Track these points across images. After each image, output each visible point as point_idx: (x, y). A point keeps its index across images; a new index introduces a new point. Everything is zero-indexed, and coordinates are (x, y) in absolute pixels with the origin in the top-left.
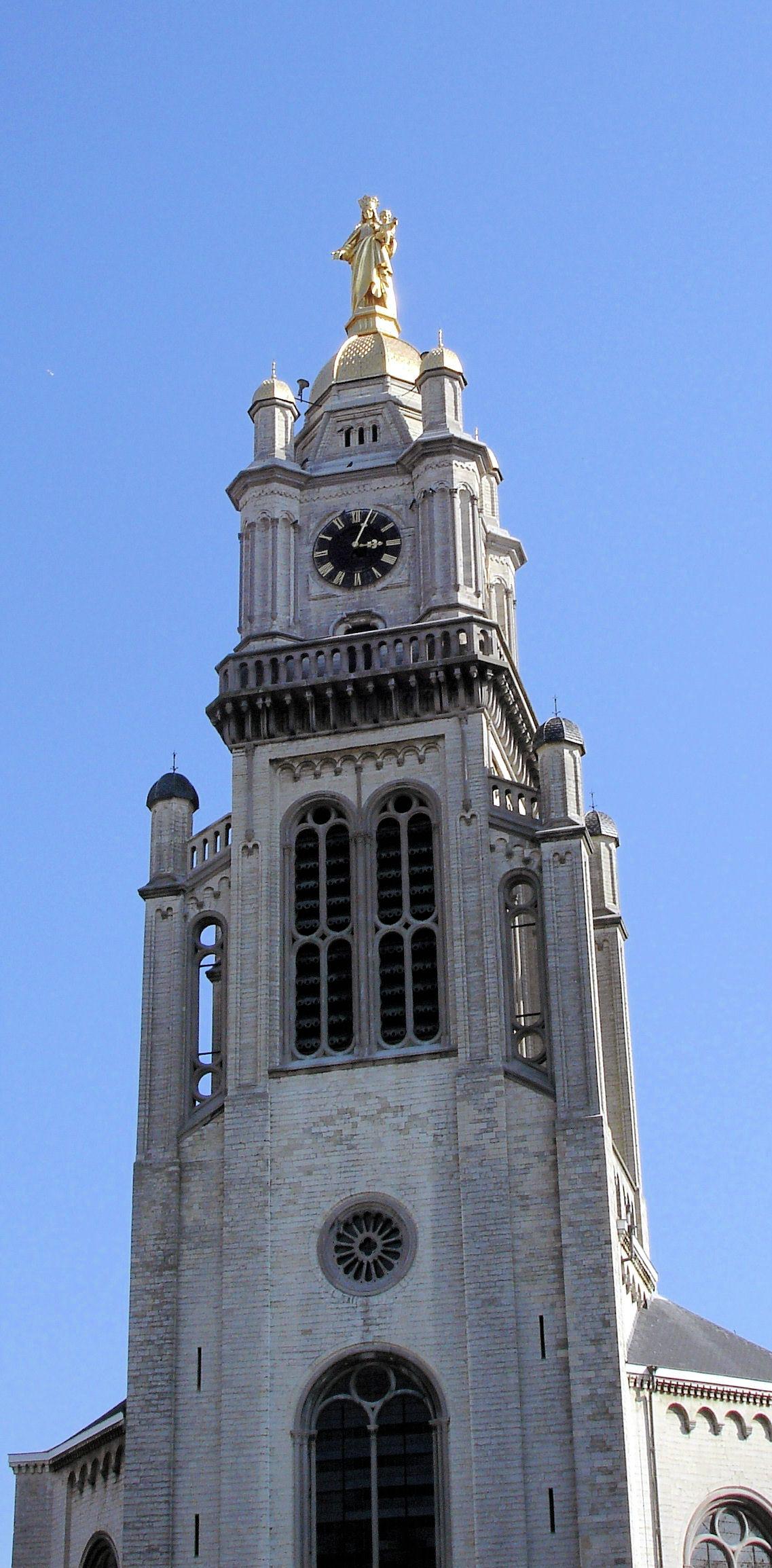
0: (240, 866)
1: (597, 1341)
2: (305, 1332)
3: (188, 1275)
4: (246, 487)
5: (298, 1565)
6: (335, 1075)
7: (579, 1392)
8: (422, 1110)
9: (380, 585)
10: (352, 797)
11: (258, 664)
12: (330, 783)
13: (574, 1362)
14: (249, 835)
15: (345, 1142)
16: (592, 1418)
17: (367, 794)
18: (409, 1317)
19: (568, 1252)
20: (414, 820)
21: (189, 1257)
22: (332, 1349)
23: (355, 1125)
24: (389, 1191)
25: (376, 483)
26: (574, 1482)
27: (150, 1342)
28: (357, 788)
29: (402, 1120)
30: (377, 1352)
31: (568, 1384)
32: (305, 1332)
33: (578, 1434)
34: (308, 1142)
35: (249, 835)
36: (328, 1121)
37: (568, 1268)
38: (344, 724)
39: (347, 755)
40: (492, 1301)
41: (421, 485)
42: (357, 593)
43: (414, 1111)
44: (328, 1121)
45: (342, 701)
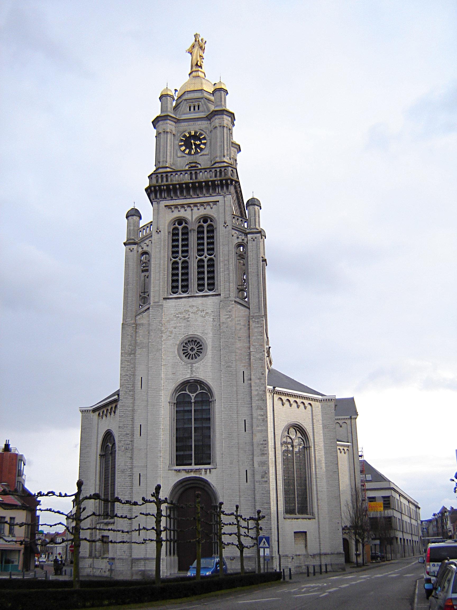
8: (209, 311)
9: (200, 154)
15: (187, 320)
16: (258, 400)
18: (204, 370)
21: (138, 351)
22: (181, 379)
23: (189, 315)
28: (192, 215)
29: (203, 314)
36: (181, 313)
39: (189, 205)
40: (229, 367)
42: (192, 156)
44: (181, 313)
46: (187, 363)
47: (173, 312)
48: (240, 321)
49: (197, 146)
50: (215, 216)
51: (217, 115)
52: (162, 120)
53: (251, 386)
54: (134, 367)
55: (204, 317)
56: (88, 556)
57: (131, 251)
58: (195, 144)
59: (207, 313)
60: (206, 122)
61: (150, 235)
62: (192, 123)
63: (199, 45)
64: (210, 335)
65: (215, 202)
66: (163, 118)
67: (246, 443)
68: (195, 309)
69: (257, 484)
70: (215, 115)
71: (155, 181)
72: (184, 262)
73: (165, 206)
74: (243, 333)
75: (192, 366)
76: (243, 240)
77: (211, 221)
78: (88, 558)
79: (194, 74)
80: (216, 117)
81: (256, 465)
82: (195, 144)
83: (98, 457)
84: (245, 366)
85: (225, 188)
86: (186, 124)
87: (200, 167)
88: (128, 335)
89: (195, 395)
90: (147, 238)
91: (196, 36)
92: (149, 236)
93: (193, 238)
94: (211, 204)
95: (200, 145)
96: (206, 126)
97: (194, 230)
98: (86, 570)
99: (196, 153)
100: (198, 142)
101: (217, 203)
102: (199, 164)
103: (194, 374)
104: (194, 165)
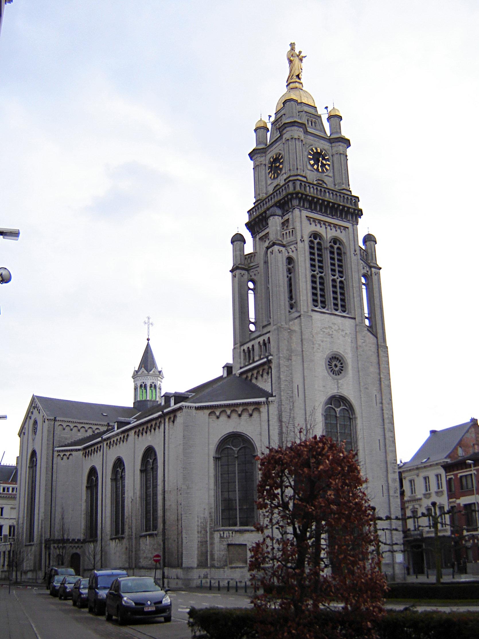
0: (300, 245)
1: (389, 404)
2: (324, 386)
3: (294, 363)
4: (286, 127)
5: (1, 230)
6: (326, 315)
7: (386, 416)
8: (348, 332)
9: (325, 174)
10: (324, 235)
11: (347, 198)
12: (321, 230)
13: (384, 408)
14: (302, 237)
15: (331, 336)
16: (389, 423)
17: (329, 236)
18: (347, 387)
19: (382, 379)
20: (338, 248)
21: (294, 358)
22: (330, 394)
23: (332, 331)
24: (341, 352)
25: (322, 142)
26: (385, 439)
27: (287, 381)
28: (328, 234)
29: (344, 333)
30: (339, 396)
31: (383, 413)
32: (324, 386)
33: (386, 427)
34: (322, 333)
35: (302, 237)
36: (326, 328)
37: (382, 383)
38: (325, 213)
39: (325, 222)
40: (367, 388)
41: (335, 149)
42: (319, 174)
43: (347, 332)
44: (326, 328)
45: (342, 211)
46: (334, 379)
47: (320, 325)
48: (371, 347)
49: (323, 165)
50: (345, 241)
51: (342, 142)
52: (297, 126)
53: (383, 410)
54: (291, 374)
55: (344, 337)
56: (196, 566)
57: (280, 252)
58: (322, 162)
59: (346, 333)
60: (328, 144)
61: (295, 242)
62: (317, 139)
63: (294, 57)
64: (350, 355)
65: (346, 228)
66: (300, 125)
67: (381, 461)
68: (336, 327)
69: (391, 498)
70: (339, 141)
71: (293, 189)
72: (321, 278)
73: (307, 216)
74: (374, 359)
75: (338, 382)
76: (368, 271)
77: (339, 244)
78: (197, 568)
79: (292, 85)
80: (340, 143)
81: (390, 481)
82: (322, 163)
83: (28, 468)
84: (376, 390)
85: (354, 217)
86: (312, 138)
87: (325, 186)
88: (285, 339)
89: (339, 409)
90: (293, 244)
91: (292, 45)
92: (293, 243)
93: (327, 255)
94: (342, 228)
95: (325, 165)
96: (328, 147)
97: (327, 248)
98: (195, 582)
99: (323, 172)
100: (324, 162)
101: (347, 229)
102: (325, 183)
103: (340, 390)
104: (321, 182)
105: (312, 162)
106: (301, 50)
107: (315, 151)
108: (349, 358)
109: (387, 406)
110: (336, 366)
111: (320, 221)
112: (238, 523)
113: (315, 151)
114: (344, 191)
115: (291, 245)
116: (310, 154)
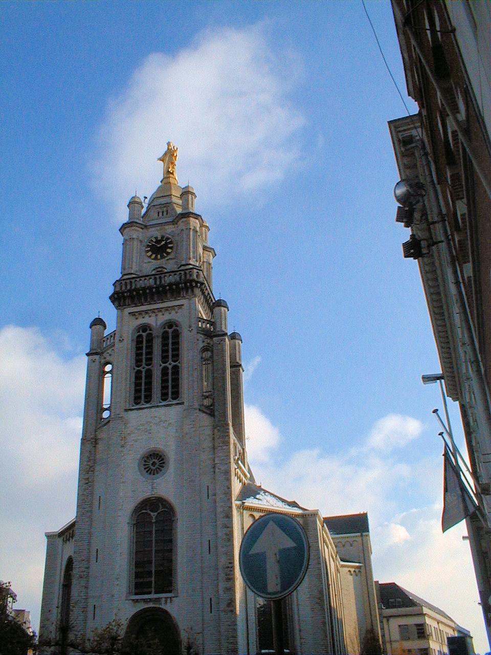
8: (172, 421)
12: (150, 320)
18: (166, 486)
28: (156, 321)
44: (142, 425)
73: (129, 313)
87: (166, 271)
102: (164, 268)
105: (169, 250)
106: (462, 538)
107: (169, 246)
108: (171, 455)
109: (223, 496)
110: (154, 464)
111: (146, 312)
112: (150, 356)
113: (169, 246)
114: (183, 268)
115: (108, 349)
116: (148, 251)
